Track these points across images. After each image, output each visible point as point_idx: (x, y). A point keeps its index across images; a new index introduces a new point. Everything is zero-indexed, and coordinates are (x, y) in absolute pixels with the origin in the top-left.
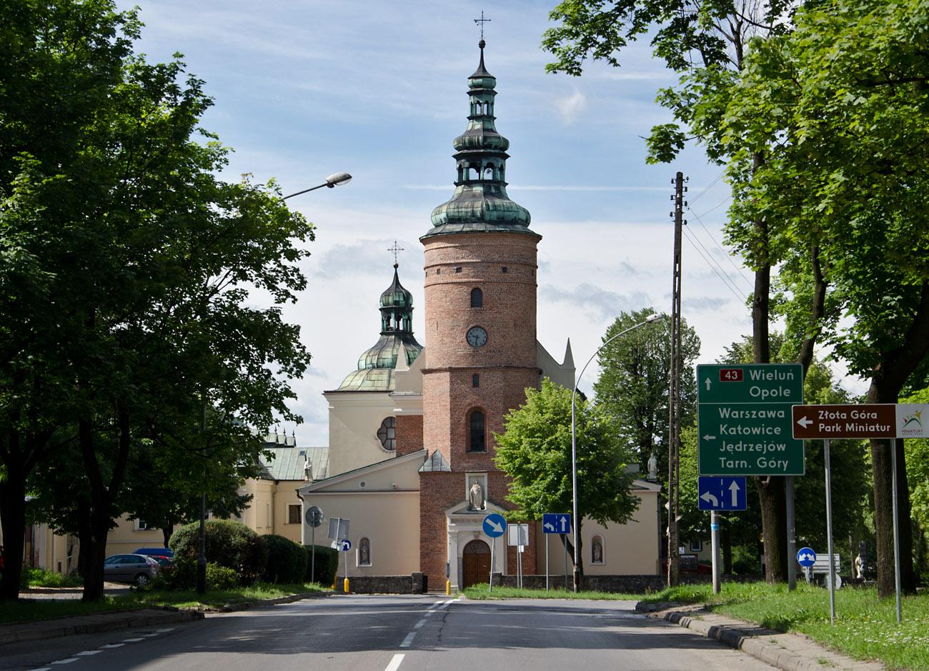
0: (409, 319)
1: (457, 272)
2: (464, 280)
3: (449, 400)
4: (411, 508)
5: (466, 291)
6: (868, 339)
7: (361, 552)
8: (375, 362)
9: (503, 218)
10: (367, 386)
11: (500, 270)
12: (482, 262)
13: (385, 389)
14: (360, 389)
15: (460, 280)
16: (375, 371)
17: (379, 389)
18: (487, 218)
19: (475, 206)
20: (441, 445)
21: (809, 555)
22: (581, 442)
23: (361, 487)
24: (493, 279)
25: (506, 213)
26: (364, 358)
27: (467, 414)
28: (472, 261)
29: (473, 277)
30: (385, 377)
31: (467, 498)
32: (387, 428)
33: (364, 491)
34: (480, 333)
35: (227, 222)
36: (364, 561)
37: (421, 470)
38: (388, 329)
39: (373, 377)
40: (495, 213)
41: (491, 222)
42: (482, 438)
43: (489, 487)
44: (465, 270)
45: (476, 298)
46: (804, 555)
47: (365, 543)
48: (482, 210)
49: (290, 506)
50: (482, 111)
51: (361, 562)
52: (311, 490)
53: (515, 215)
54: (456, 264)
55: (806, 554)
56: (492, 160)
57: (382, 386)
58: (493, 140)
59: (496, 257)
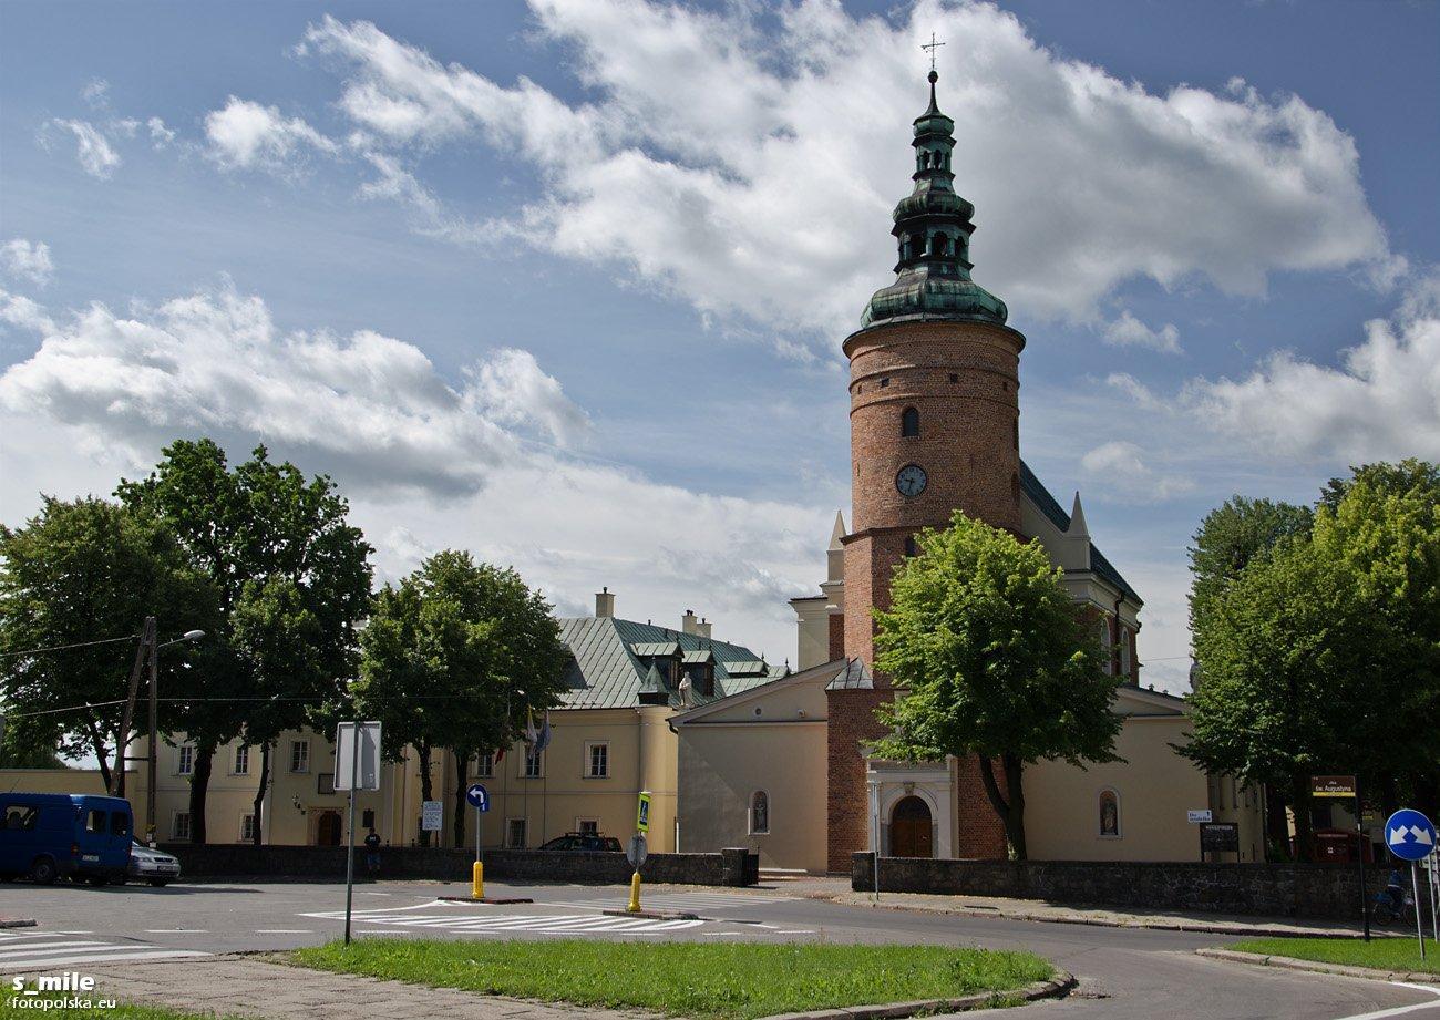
1: (883, 386)
2: (891, 397)
3: (870, 580)
4: (816, 744)
5: (895, 411)
6: (836, 361)
7: (755, 813)
12: (918, 367)
15: (887, 398)
18: (928, 304)
21: (1415, 830)
22: (40, 591)
23: (760, 707)
25: (958, 297)
28: (903, 367)
29: (905, 391)
33: (759, 721)
34: (916, 475)
35: (188, 295)
37: (830, 687)
41: (934, 310)
44: (893, 382)
45: (910, 422)
46: (1403, 830)
47: (761, 802)
48: (920, 294)
51: (756, 827)
52: (686, 720)
54: (880, 375)
55: (1409, 827)
58: (944, 199)
59: (940, 359)
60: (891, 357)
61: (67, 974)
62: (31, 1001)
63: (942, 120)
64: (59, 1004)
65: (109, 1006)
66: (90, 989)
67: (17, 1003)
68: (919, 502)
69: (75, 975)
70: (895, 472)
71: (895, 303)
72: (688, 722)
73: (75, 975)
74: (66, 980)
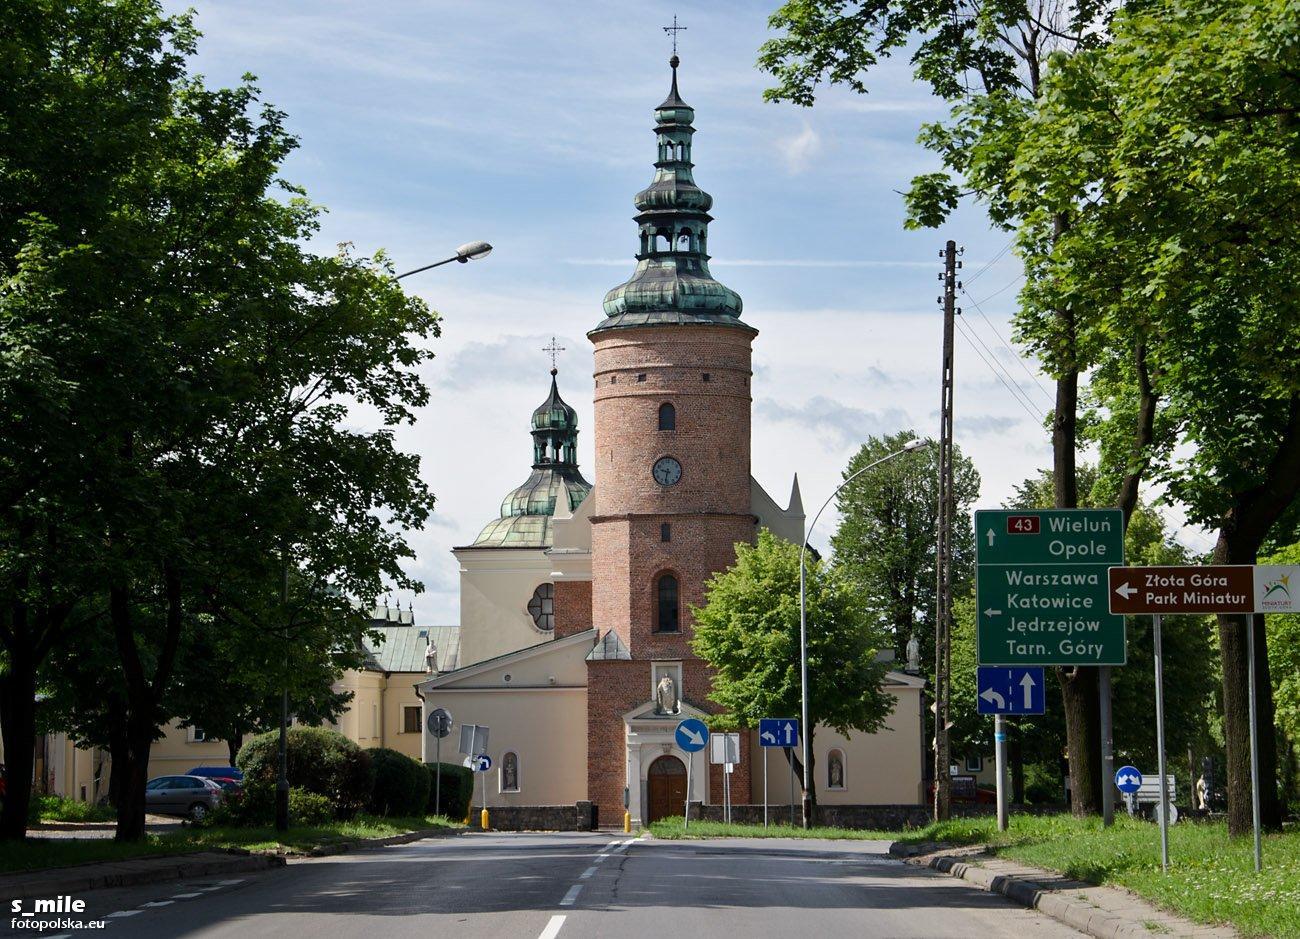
0: (573, 446)
4: (573, 712)
5: (652, 407)
7: (505, 772)
8: (525, 506)
9: (704, 305)
10: (514, 540)
11: (700, 378)
13: (538, 544)
14: (503, 545)
15: (644, 392)
16: (525, 519)
17: (531, 545)
18: (682, 305)
19: (665, 288)
20: (617, 623)
24: (690, 390)
25: (709, 299)
26: (509, 500)
27: (653, 580)
29: (662, 387)
30: (539, 527)
31: (654, 697)
32: (541, 599)
33: (509, 687)
34: (671, 466)
36: (510, 786)
37: (590, 658)
38: (542, 461)
39: (522, 528)
40: (693, 299)
41: (687, 311)
42: (675, 613)
43: (684, 682)
44: (651, 379)
45: (666, 417)
47: (510, 760)
48: (675, 295)
49: (406, 708)
50: (674, 155)
51: (505, 786)
52: (435, 686)
54: (637, 370)
56: (688, 224)
57: (535, 540)
59: (694, 360)
60: (648, 354)
61: (60, 897)
62: (28, 921)
63: (686, 111)
64: (53, 924)
65: (99, 927)
66: (82, 910)
67: (16, 924)
68: (675, 491)
69: (68, 898)
70: (652, 462)
71: (648, 299)
72: (434, 688)
73: (68, 898)
74: (60, 903)
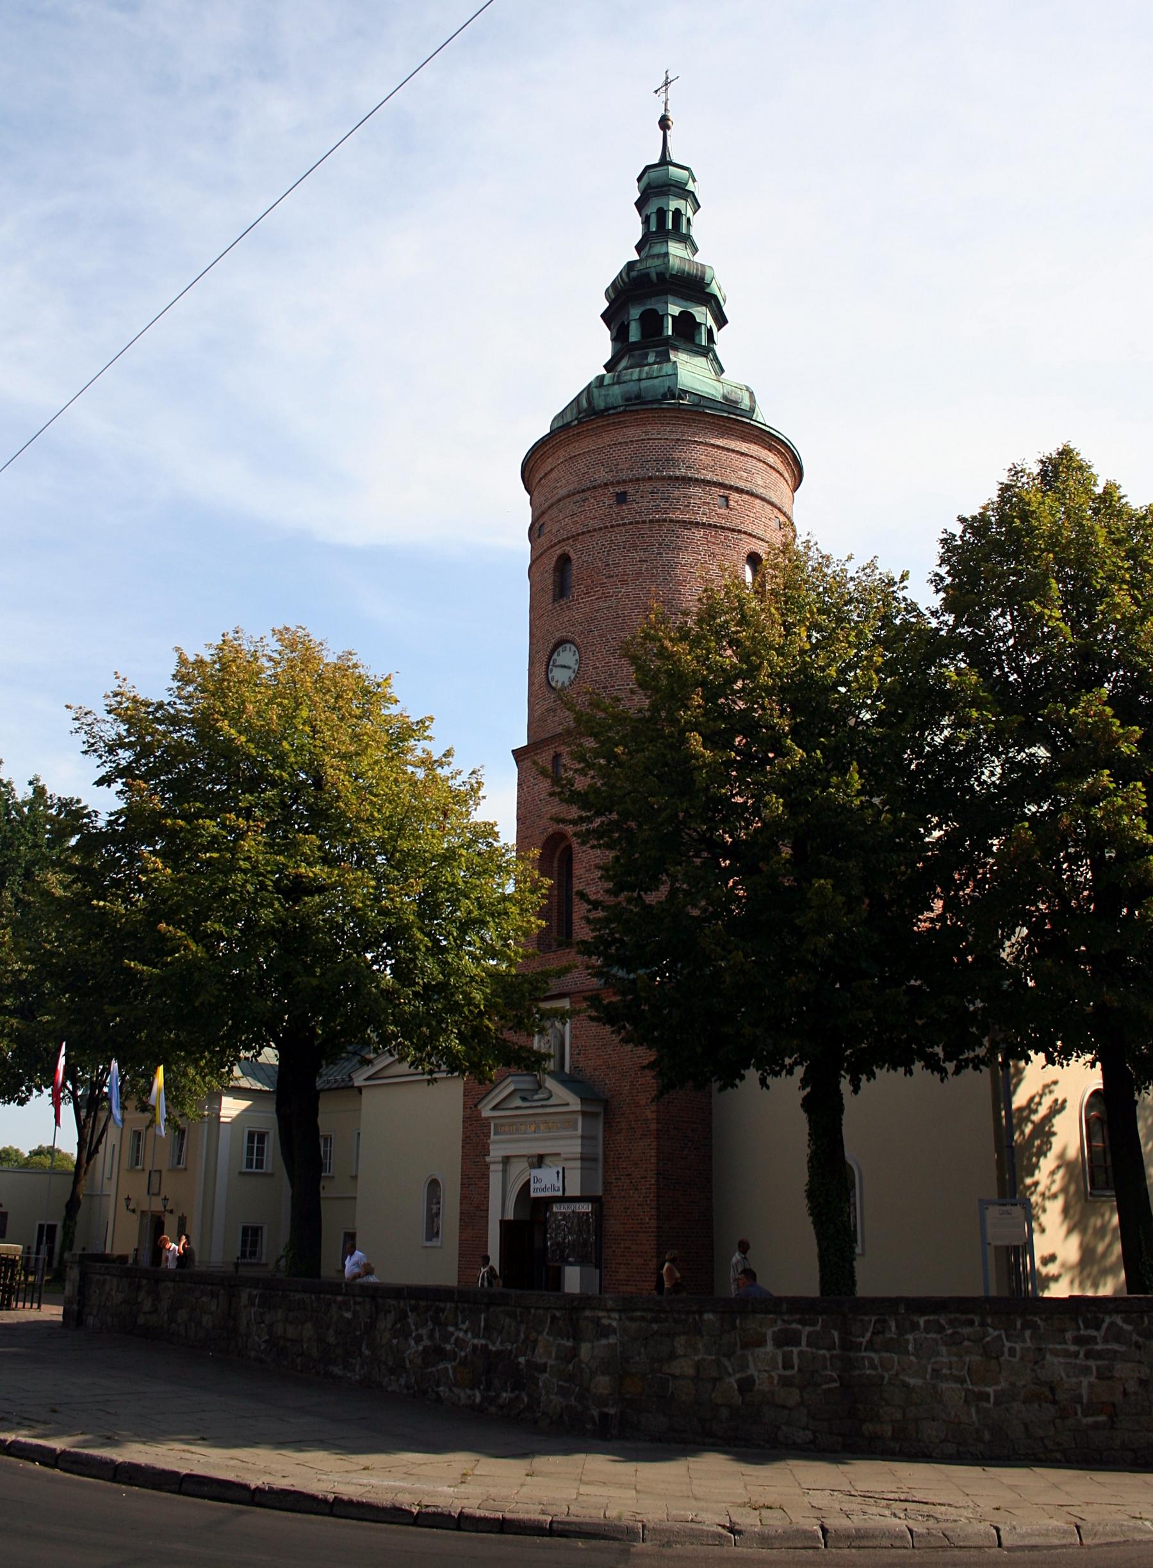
25: (644, 384)
53: (667, 384)
59: (602, 475)
